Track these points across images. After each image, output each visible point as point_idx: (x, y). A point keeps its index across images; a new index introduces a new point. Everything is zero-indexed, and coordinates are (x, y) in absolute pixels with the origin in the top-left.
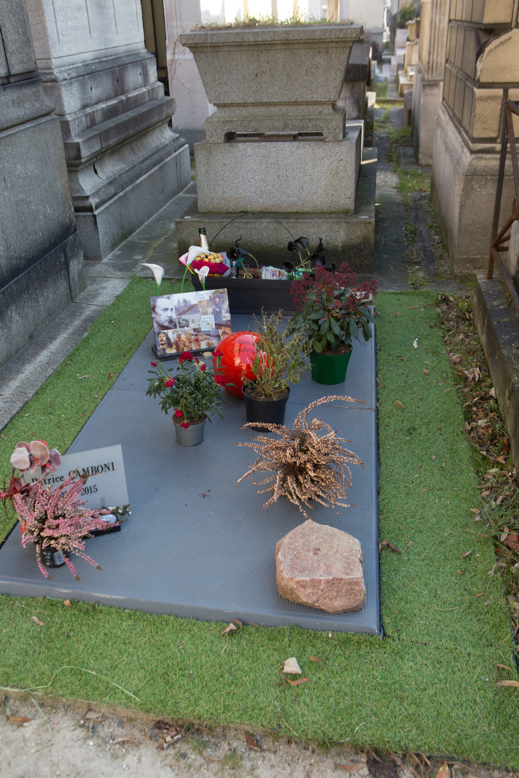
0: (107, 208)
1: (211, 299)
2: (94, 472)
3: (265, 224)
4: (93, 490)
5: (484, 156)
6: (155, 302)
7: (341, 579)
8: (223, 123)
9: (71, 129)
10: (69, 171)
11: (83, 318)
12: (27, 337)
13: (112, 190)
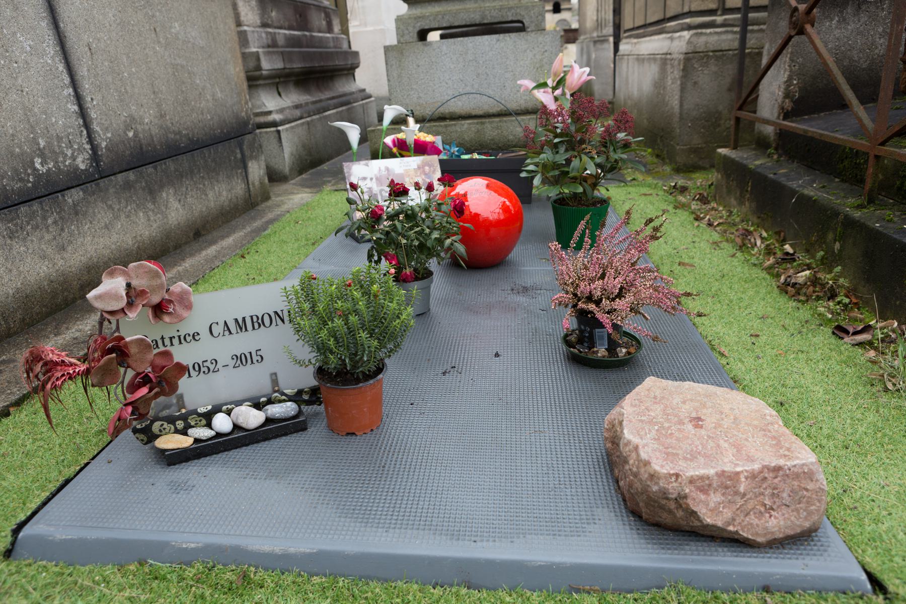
0: (292, 128)
1: (419, 168)
2: (256, 325)
3: (466, 126)
4: (255, 358)
5: (704, 31)
6: (350, 169)
7: (778, 469)
8: (415, 18)
9: (250, 39)
10: (250, 87)
11: (263, 220)
12: (191, 235)
13: (298, 113)
